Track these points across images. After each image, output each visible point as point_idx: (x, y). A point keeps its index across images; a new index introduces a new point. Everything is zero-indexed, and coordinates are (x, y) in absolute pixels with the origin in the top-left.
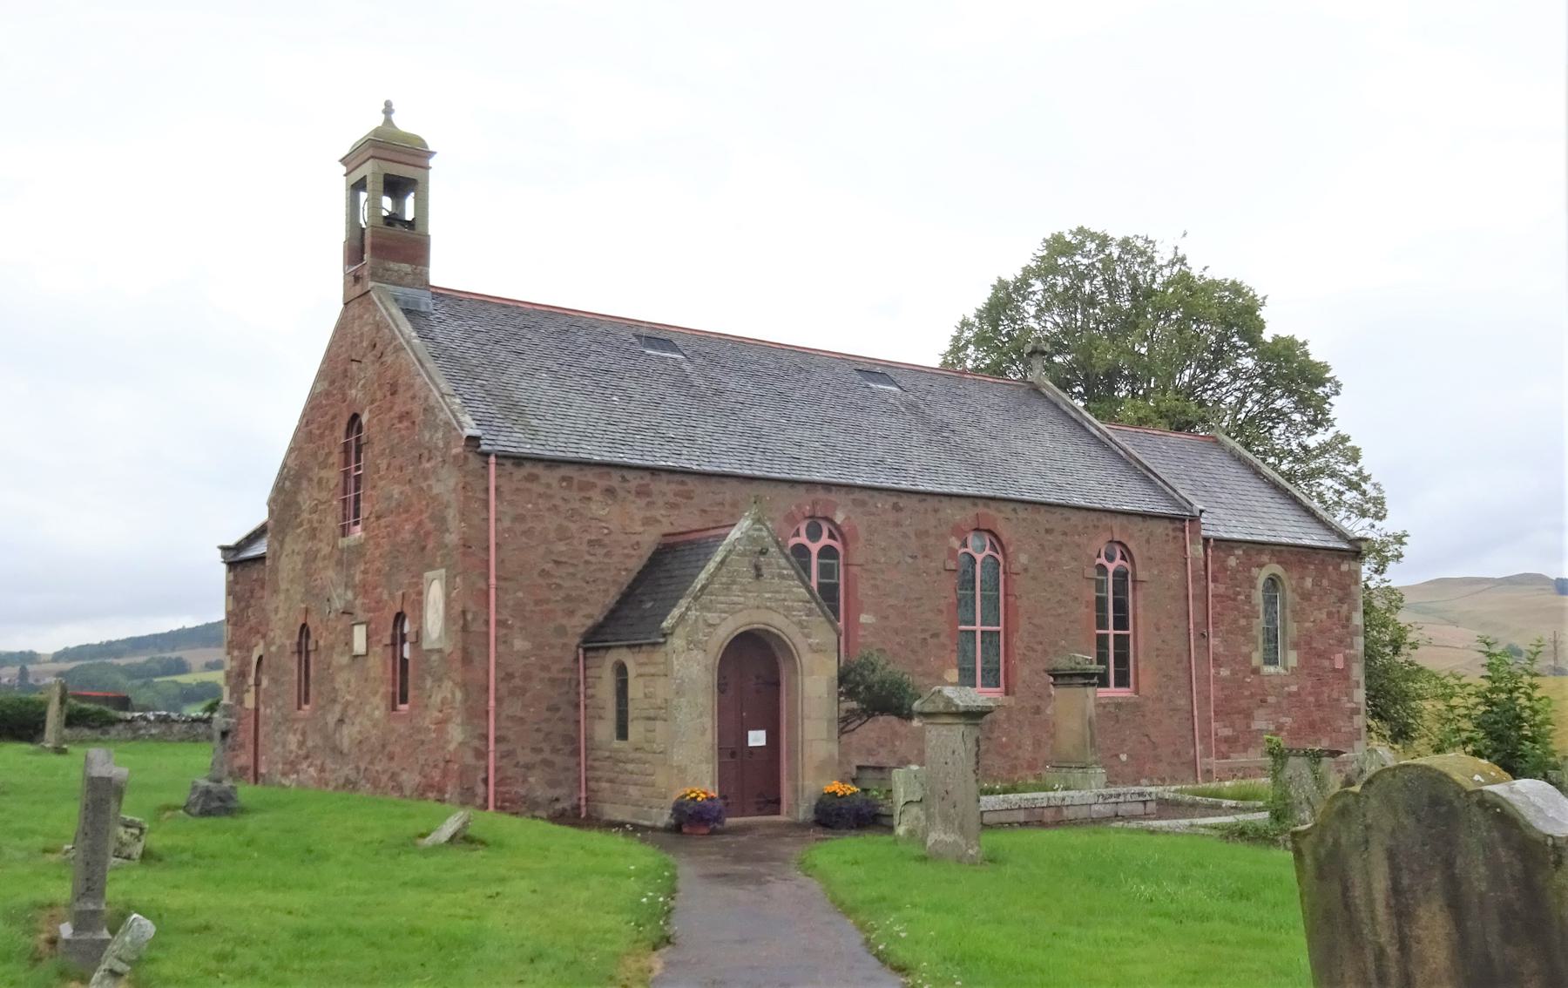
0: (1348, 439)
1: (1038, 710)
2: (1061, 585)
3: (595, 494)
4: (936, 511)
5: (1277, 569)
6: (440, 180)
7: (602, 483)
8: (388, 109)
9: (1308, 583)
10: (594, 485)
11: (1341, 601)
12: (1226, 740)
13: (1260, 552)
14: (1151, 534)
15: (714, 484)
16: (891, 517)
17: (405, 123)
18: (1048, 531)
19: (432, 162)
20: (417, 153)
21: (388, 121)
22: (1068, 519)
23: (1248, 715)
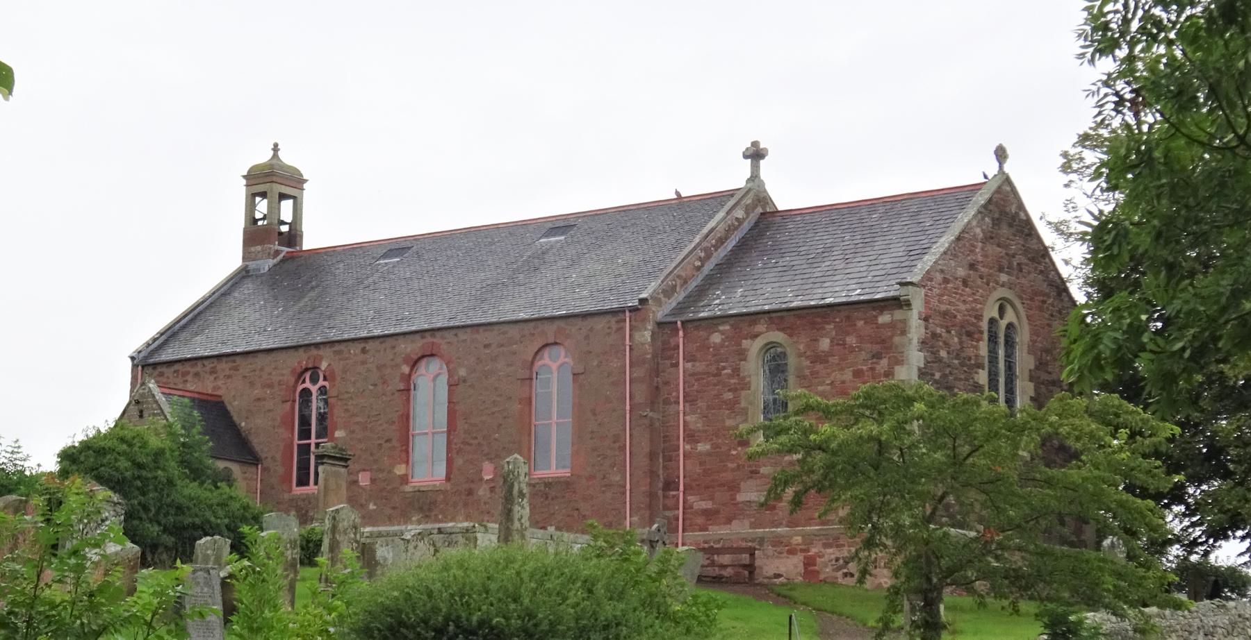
0: (1065, 155)
1: (470, 492)
2: (496, 389)
3: (189, 378)
4: (394, 347)
5: (778, 336)
6: (309, 195)
7: (193, 370)
8: (276, 148)
9: (825, 344)
10: (188, 373)
11: (877, 356)
12: (706, 513)
13: (754, 323)
14: (591, 330)
15: (250, 359)
16: (361, 357)
17: (287, 158)
18: (486, 346)
19: (305, 186)
20: (297, 180)
21: (275, 156)
22: (504, 333)
23: (734, 487)
